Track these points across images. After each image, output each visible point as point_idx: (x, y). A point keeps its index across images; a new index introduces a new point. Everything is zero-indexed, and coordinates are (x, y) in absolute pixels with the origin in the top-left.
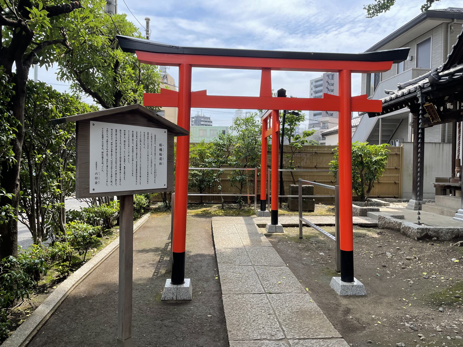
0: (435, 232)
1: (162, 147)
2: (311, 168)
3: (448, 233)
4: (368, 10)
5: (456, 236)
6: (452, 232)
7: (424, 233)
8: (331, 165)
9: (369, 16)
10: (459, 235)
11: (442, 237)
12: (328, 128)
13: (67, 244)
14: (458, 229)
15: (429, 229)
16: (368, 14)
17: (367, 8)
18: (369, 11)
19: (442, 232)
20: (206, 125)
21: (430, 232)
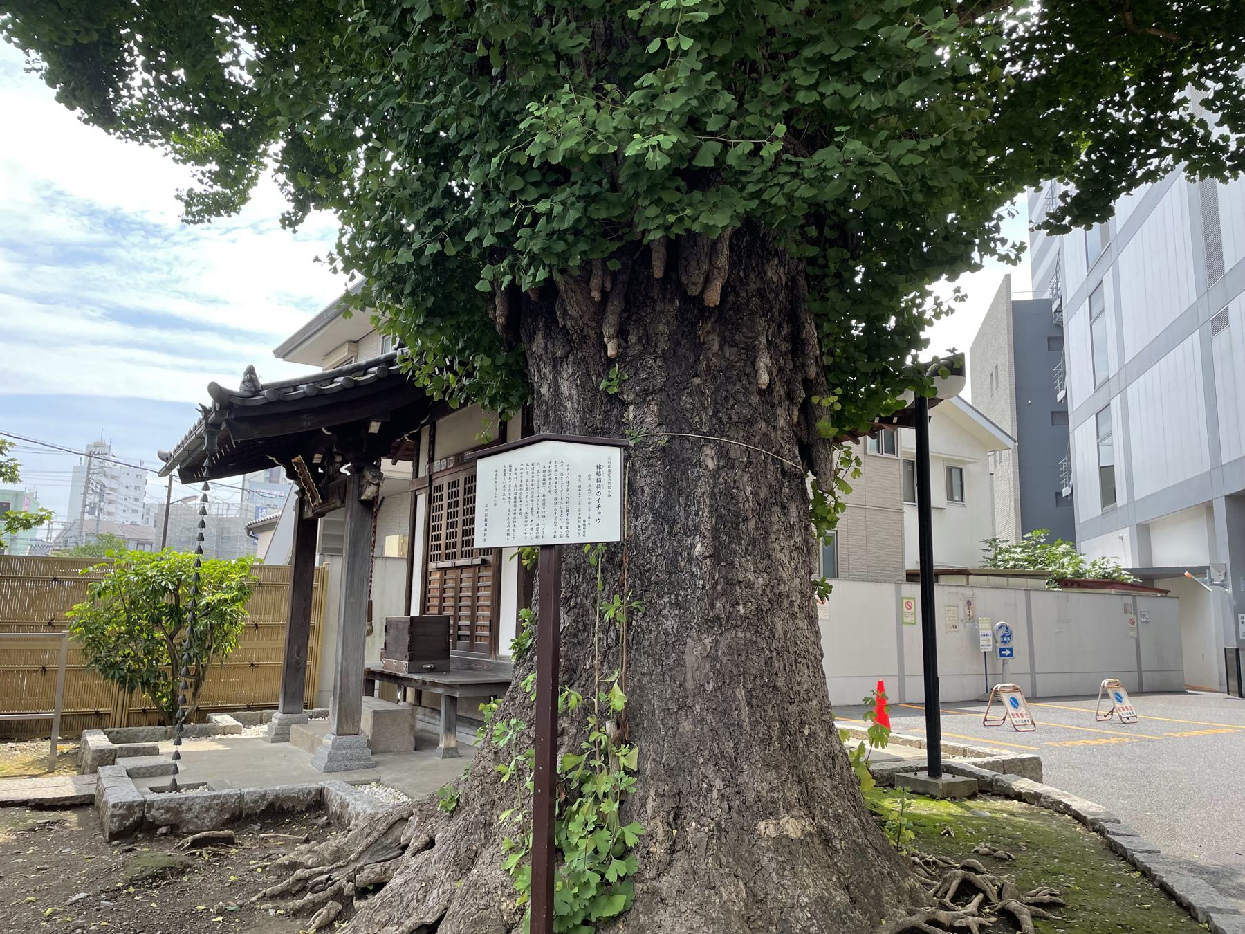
0: (168, 810)
1: (203, 544)
2: (37, 626)
3: (208, 809)
4: (186, 202)
5: (233, 815)
6: (223, 804)
7: (135, 817)
8: (73, 619)
9: (190, 218)
10: (241, 813)
11: (188, 822)
12: (1039, 780)
13: (807, 164)
14: (241, 796)
15: (151, 805)
16: (187, 213)
17: (186, 198)
18: (188, 204)
19: (190, 809)
20: (95, 342)
21: (153, 812)
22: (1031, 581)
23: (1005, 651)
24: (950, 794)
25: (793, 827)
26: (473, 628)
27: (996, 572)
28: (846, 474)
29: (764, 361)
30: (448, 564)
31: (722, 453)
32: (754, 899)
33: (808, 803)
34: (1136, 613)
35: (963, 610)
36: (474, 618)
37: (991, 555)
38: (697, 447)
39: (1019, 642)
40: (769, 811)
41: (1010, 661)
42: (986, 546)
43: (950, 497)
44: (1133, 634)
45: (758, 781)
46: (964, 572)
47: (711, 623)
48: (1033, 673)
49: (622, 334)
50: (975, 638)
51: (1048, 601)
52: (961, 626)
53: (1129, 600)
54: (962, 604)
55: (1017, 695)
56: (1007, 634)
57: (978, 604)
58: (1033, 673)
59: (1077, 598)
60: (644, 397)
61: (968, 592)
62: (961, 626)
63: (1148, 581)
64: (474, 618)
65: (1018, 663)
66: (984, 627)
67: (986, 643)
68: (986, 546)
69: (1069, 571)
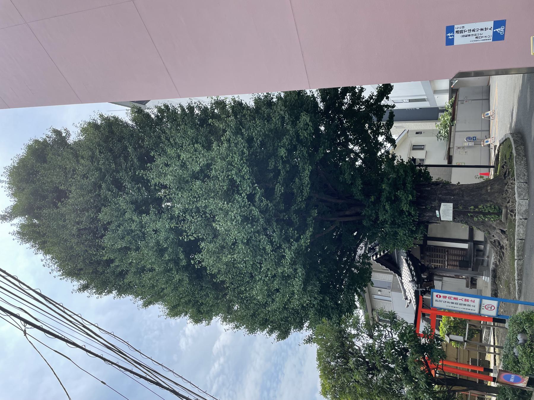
22: (453, 130)
23: (474, 139)
24: (497, 165)
25: (489, 188)
26: (462, 256)
27: (449, 137)
28: (441, 180)
29: (427, 189)
30: (446, 262)
31: (439, 194)
32: (497, 192)
33: (487, 186)
34: (463, 101)
35: (461, 150)
36: (459, 256)
37: (442, 138)
38: (438, 197)
39: (471, 135)
40: (487, 190)
41: (477, 138)
42: (439, 140)
43: (423, 149)
44: (470, 101)
45: (483, 191)
46: (449, 148)
47: (463, 196)
48: (481, 131)
49: (423, 206)
50: (469, 147)
51: (459, 125)
52: (466, 151)
53: (459, 102)
54: (459, 150)
55: (485, 141)
56: (469, 139)
57: (459, 145)
58: (481, 131)
59: (459, 115)
60: (432, 204)
61: (455, 148)
62: (466, 151)
63: (453, 92)
64: (459, 256)
65: (478, 135)
66: (466, 144)
67: (471, 144)
68: (439, 140)
69: (449, 117)
